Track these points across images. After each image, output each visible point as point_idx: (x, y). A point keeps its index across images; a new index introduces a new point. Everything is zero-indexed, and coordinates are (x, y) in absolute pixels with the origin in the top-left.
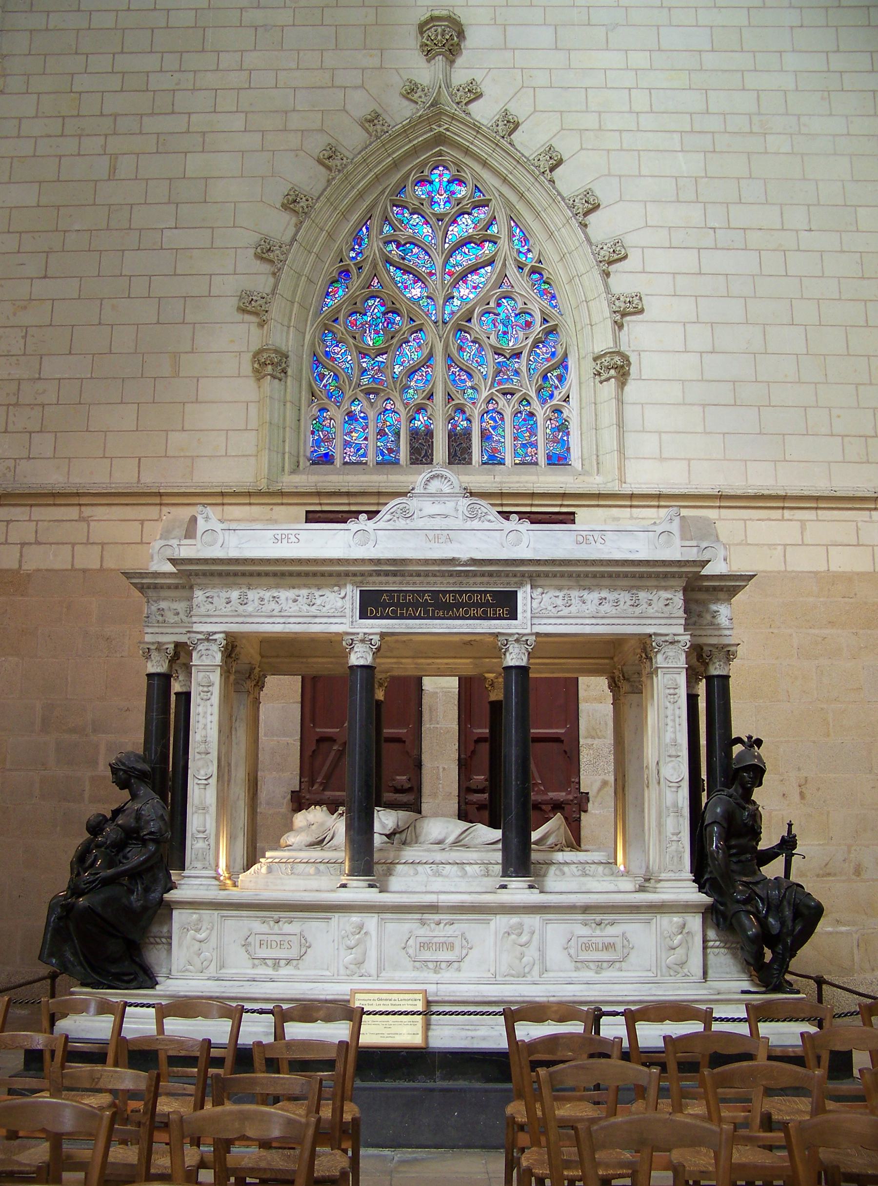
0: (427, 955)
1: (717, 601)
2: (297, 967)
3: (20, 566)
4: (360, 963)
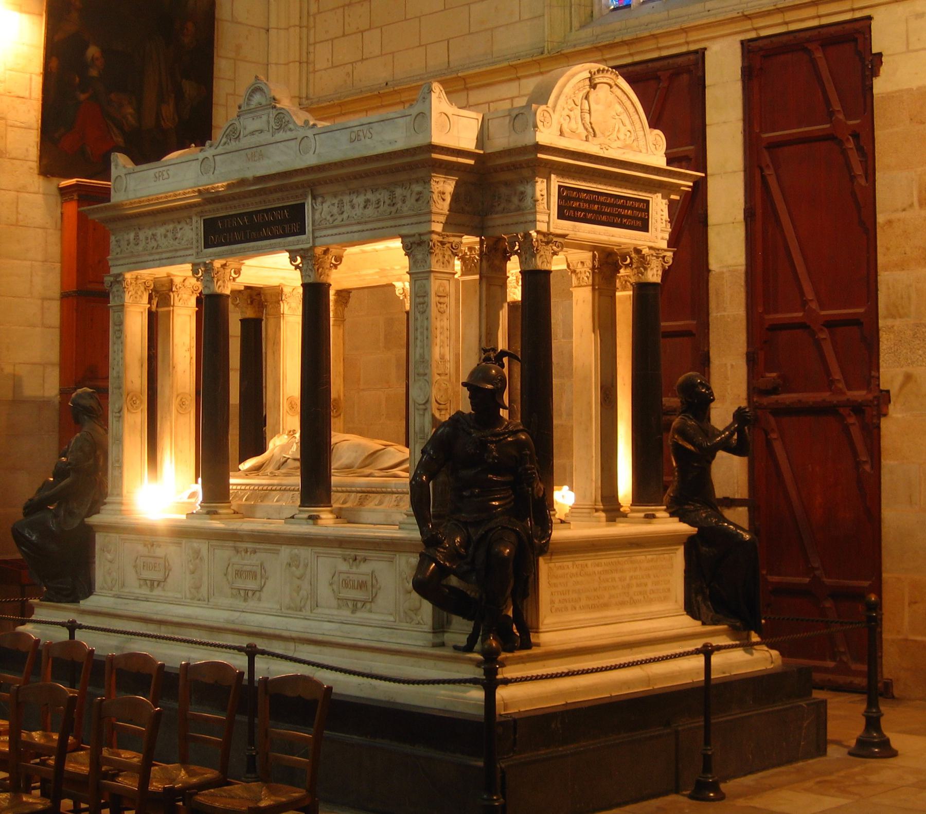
0: (240, 584)
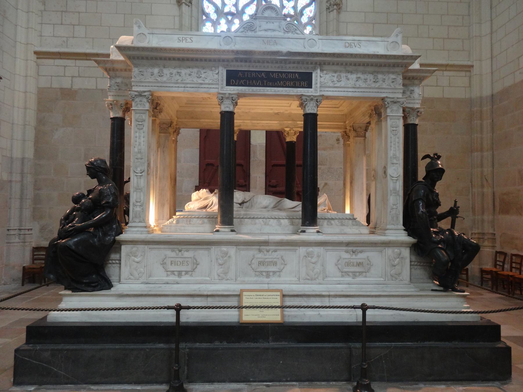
0: (262, 268)
1: (414, 85)
2: (191, 275)
3: (72, 87)
4: (226, 273)
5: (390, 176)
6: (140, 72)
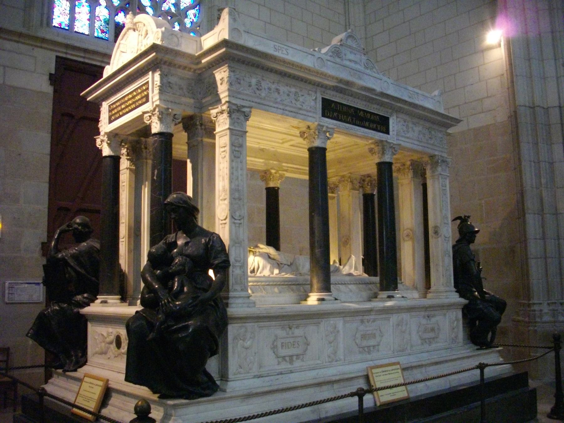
2: (303, 360)
5: (444, 236)
6: (237, 79)
